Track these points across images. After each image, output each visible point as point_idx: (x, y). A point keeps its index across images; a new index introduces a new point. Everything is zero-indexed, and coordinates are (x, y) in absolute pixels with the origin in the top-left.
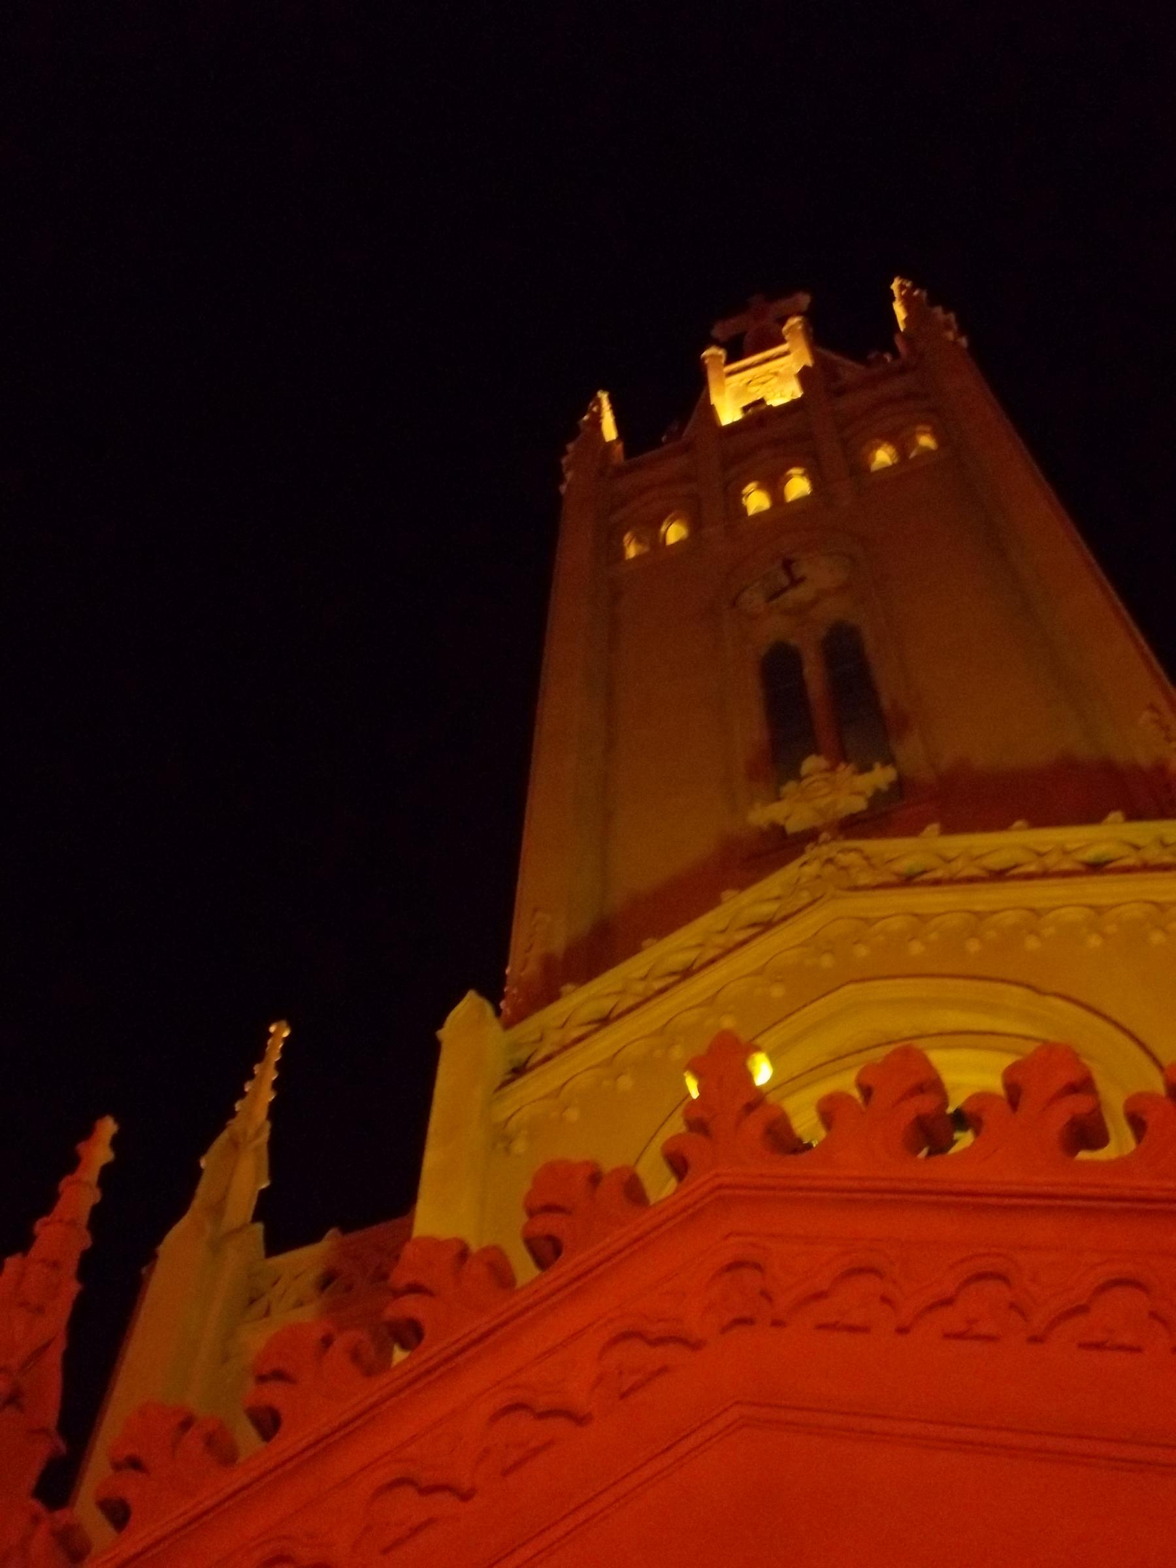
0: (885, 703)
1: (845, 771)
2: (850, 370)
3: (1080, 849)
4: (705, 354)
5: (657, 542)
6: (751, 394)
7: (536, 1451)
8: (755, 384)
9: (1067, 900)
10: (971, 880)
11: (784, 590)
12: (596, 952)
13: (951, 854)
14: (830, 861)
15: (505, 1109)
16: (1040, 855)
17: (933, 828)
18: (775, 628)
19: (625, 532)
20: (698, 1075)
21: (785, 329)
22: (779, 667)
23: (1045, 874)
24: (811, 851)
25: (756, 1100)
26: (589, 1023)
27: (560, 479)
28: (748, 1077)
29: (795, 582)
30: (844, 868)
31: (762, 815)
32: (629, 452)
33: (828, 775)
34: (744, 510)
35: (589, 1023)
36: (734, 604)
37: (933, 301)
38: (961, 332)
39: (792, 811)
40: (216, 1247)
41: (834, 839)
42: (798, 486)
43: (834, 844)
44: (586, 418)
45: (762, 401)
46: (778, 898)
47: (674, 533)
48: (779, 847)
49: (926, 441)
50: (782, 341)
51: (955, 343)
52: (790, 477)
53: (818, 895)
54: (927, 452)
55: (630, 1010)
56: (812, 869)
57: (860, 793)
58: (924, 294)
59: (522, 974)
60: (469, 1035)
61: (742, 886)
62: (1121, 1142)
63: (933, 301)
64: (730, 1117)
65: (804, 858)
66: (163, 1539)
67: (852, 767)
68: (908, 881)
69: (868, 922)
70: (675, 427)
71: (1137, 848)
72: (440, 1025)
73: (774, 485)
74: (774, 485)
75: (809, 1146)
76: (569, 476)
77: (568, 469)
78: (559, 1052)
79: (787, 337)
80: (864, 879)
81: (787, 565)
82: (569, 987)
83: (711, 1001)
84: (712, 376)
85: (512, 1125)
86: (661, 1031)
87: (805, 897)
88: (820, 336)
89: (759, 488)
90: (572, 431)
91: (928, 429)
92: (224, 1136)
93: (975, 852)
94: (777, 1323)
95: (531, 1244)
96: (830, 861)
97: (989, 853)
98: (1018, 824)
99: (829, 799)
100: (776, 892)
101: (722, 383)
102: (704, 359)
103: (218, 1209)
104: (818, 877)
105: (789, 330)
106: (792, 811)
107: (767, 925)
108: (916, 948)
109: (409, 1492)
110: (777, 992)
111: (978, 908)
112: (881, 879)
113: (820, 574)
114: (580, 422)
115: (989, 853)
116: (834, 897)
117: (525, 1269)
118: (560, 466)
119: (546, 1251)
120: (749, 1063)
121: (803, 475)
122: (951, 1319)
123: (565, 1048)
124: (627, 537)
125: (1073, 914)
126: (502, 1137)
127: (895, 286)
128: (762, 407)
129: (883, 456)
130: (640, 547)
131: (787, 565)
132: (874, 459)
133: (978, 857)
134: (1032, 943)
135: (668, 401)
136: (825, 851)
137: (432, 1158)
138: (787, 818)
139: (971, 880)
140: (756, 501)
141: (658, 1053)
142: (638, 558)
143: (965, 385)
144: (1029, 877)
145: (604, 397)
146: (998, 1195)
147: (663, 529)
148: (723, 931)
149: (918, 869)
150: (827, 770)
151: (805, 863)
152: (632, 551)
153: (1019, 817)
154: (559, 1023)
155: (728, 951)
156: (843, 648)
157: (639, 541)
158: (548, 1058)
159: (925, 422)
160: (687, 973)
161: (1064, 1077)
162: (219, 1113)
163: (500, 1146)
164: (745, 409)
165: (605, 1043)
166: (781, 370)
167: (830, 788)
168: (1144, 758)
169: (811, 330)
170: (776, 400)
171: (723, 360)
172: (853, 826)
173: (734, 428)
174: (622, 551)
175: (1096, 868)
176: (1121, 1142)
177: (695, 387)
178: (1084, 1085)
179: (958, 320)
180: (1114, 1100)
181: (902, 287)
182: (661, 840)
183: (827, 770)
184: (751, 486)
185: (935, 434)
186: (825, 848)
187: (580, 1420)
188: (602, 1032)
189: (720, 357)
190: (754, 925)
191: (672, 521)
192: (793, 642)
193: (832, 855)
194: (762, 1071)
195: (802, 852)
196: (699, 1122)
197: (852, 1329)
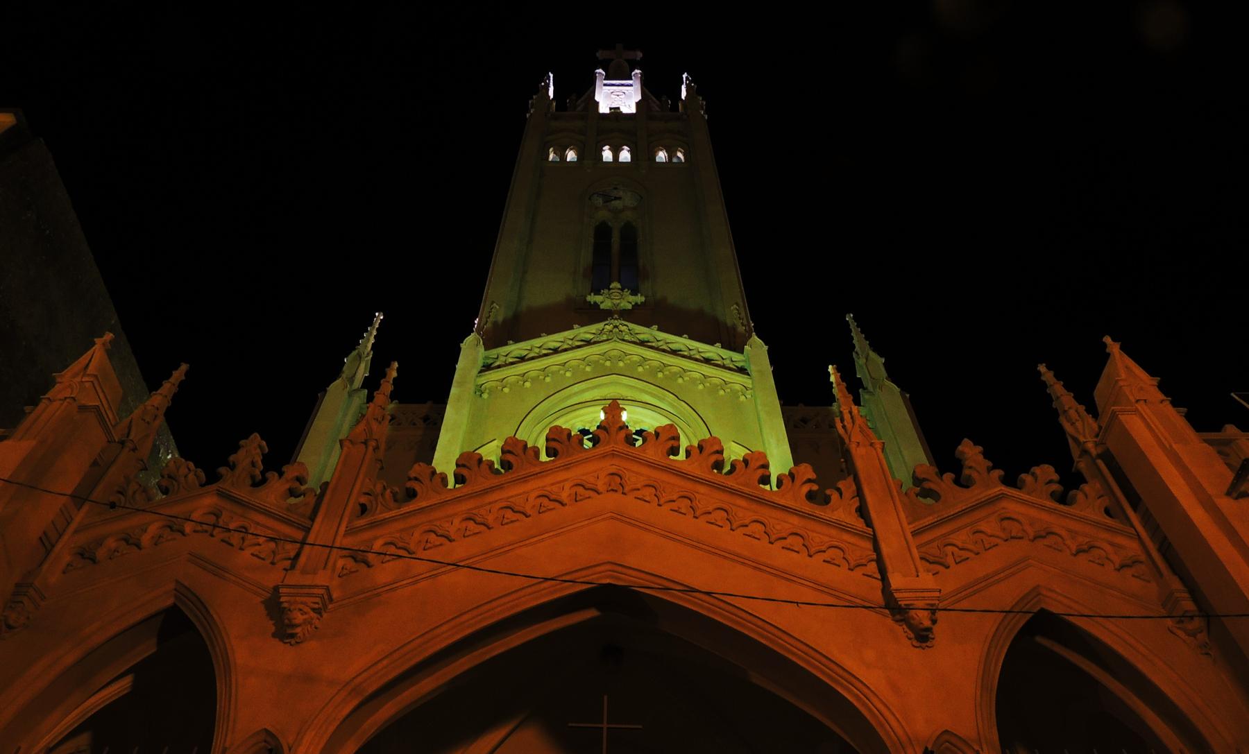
1: (627, 292)
5: (563, 157)
8: (618, 97)
10: (664, 351)
14: (616, 327)
15: (481, 380)
18: (603, 215)
22: (602, 232)
23: (690, 358)
27: (528, 110)
31: (592, 298)
38: (706, 112)
39: (604, 301)
40: (350, 394)
42: (607, 155)
48: (595, 315)
49: (680, 155)
55: (533, 358)
60: (471, 351)
62: (682, 456)
64: (612, 427)
68: (642, 343)
80: (627, 338)
87: (605, 337)
88: (646, 86)
92: (354, 353)
96: (616, 327)
103: (351, 380)
106: (604, 301)
107: (588, 343)
108: (640, 369)
110: (588, 369)
122: (674, 506)
123: (506, 365)
126: (479, 390)
127: (685, 76)
134: (680, 381)
136: (616, 323)
137: (454, 391)
139: (664, 351)
144: (684, 356)
152: (551, 156)
155: (572, 348)
156: (629, 233)
158: (499, 367)
160: (556, 351)
161: (716, 448)
162: (352, 344)
167: (615, 298)
168: (729, 322)
170: (625, 110)
172: (627, 315)
175: (707, 361)
176: (682, 456)
177: (589, 87)
180: (684, 443)
182: (547, 290)
184: (607, 147)
187: (563, 505)
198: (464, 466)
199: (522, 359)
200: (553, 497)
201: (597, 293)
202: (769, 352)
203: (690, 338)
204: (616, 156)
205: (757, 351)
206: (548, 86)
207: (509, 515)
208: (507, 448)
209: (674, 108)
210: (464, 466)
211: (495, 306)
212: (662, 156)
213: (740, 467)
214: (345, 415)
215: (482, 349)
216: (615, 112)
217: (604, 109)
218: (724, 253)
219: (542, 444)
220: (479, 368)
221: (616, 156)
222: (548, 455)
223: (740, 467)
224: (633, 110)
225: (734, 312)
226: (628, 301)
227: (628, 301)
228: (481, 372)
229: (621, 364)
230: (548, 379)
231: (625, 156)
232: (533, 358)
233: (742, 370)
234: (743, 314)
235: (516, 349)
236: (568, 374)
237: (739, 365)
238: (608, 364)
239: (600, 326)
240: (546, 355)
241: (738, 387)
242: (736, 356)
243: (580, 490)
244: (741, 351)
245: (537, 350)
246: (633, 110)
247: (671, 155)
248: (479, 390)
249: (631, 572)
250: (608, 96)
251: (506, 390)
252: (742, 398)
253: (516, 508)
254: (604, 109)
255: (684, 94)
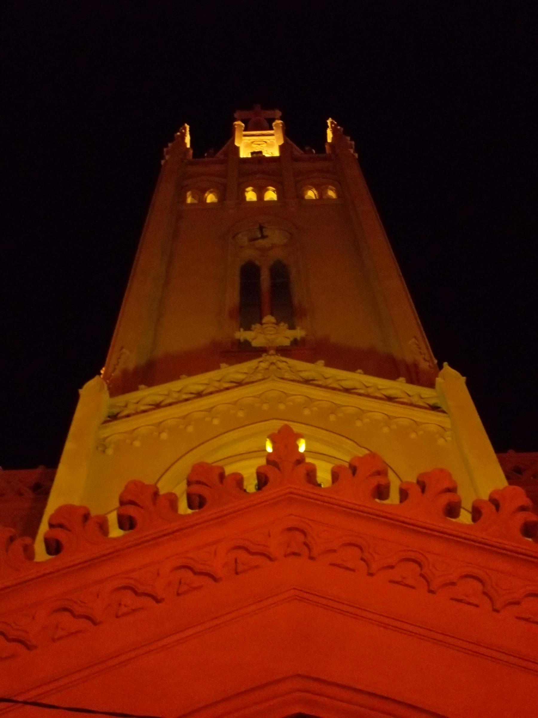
0: (296, 301)
1: (283, 326)
2: (298, 151)
3: (383, 389)
4: (236, 123)
5: (202, 201)
6: (253, 147)
7: (195, 588)
9: (378, 410)
10: (334, 389)
11: (258, 239)
12: (149, 373)
13: (327, 376)
14: (273, 363)
16: (367, 387)
17: (321, 362)
18: (249, 254)
19: (189, 190)
20: (274, 442)
21: (274, 124)
22: (249, 273)
24: (264, 356)
25: (300, 460)
26: (150, 405)
27: (163, 157)
28: (297, 447)
29: (263, 237)
30: (279, 368)
31: (242, 335)
32: (195, 156)
33: (275, 326)
34: (244, 198)
35: (150, 405)
36: (234, 237)
37: (346, 133)
38: (356, 151)
39: (255, 337)
41: (277, 354)
42: (251, 196)
43: (276, 356)
44: (178, 134)
45: (261, 152)
46: (245, 373)
47: (211, 198)
48: (243, 352)
49: (331, 194)
50: (271, 129)
51: (354, 156)
52: (268, 190)
53: (266, 377)
54: (330, 199)
56: (263, 365)
57: (288, 338)
58: (342, 129)
59: (113, 374)
60: (93, 397)
61: (231, 364)
62: (465, 517)
63: (346, 133)
64: (284, 465)
65: (261, 359)
66: (8, 587)
67: (286, 325)
68: (307, 382)
69: (287, 395)
70: (212, 151)
71: (409, 396)
72: (81, 387)
73: (260, 191)
74: (260, 191)
75: (320, 485)
76: (167, 157)
77: (167, 154)
78: (134, 414)
79: (274, 128)
80: (287, 376)
81: (261, 228)
82: (142, 386)
83: (210, 410)
84: (237, 134)
85: (108, 440)
86: (184, 417)
87: (260, 376)
88: (287, 133)
89: (253, 190)
90: (172, 139)
91: (333, 188)
93: (339, 378)
94: (312, 558)
95: (189, 497)
96: (273, 363)
97: (345, 380)
98: (359, 371)
99: (273, 337)
100: (246, 370)
101: (241, 140)
102: (235, 125)
104: (267, 369)
105: (275, 125)
106: (255, 337)
107: (239, 384)
108: (307, 412)
109: (129, 593)
110: (241, 414)
111: (338, 402)
112: (294, 378)
113: (275, 237)
114: (175, 135)
115: (345, 380)
116: (273, 380)
117: (183, 508)
118: (163, 151)
119: (196, 501)
120: (298, 442)
121: (274, 191)
123: (137, 413)
124: (189, 193)
125: (379, 416)
126: (102, 446)
127: (329, 121)
128: (259, 155)
129: (311, 194)
130: (193, 199)
131: (261, 228)
132: (306, 194)
133: (338, 380)
135: (216, 139)
137: (69, 446)
138: (253, 339)
139: (334, 389)
140: (251, 196)
141: (181, 427)
142: (192, 204)
143: (354, 173)
144: (360, 395)
145: (188, 127)
146: (421, 527)
147: (206, 195)
148: (219, 381)
149: (311, 378)
150: (273, 323)
151: (261, 362)
152: (189, 200)
153: (360, 368)
154: (135, 401)
156: (280, 272)
157: (193, 197)
158: (128, 416)
159: (334, 186)
160: (199, 395)
163: (101, 449)
164: (252, 153)
165: (158, 415)
166: (268, 141)
167: (269, 332)
169: (285, 128)
171: (243, 129)
173: (245, 160)
174: (185, 199)
175: (390, 399)
178: (452, 490)
179: (355, 145)
181: (332, 123)
183: (273, 323)
184: (250, 189)
185: (337, 192)
186: (272, 357)
187: (215, 580)
188: (156, 411)
189: (242, 126)
190: (232, 382)
191: (211, 192)
192: (257, 263)
193: (274, 361)
194: (302, 447)
195: (260, 356)
196: (271, 461)
197: (347, 568)
198: (61, 526)
199: (158, 406)
200: (198, 567)
201: (248, 328)
202: (469, 384)
203: (367, 372)
204: (260, 196)
205: (452, 383)
206: (183, 136)
207: (128, 598)
208: (129, 497)
209: (323, 150)
210: (61, 526)
211: (126, 349)
212: (311, 194)
213: (488, 510)
214: (361, 706)
215: (106, 395)
216: (257, 157)
217: (244, 153)
218: (393, 285)
219: (181, 490)
220: (103, 419)
221: (260, 196)
222: (190, 506)
223: (488, 510)
224: (276, 153)
225: (414, 346)
226: (285, 336)
227: (285, 336)
228: (106, 422)
229: (282, 407)
230: (190, 429)
231: (271, 195)
232: (170, 404)
233: (435, 408)
234: (424, 350)
235: (147, 394)
236: (216, 422)
237: (432, 402)
238: (265, 407)
239: (253, 363)
240: (187, 400)
241: (433, 428)
242: (426, 392)
243: (243, 556)
244: (431, 385)
245: (175, 395)
246: (276, 153)
247: (321, 193)
248: (102, 446)
249: (333, 691)
250: (248, 146)
251: (137, 444)
252: (441, 441)
253: (141, 589)
254: (244, 153)
255: (329, 140)
